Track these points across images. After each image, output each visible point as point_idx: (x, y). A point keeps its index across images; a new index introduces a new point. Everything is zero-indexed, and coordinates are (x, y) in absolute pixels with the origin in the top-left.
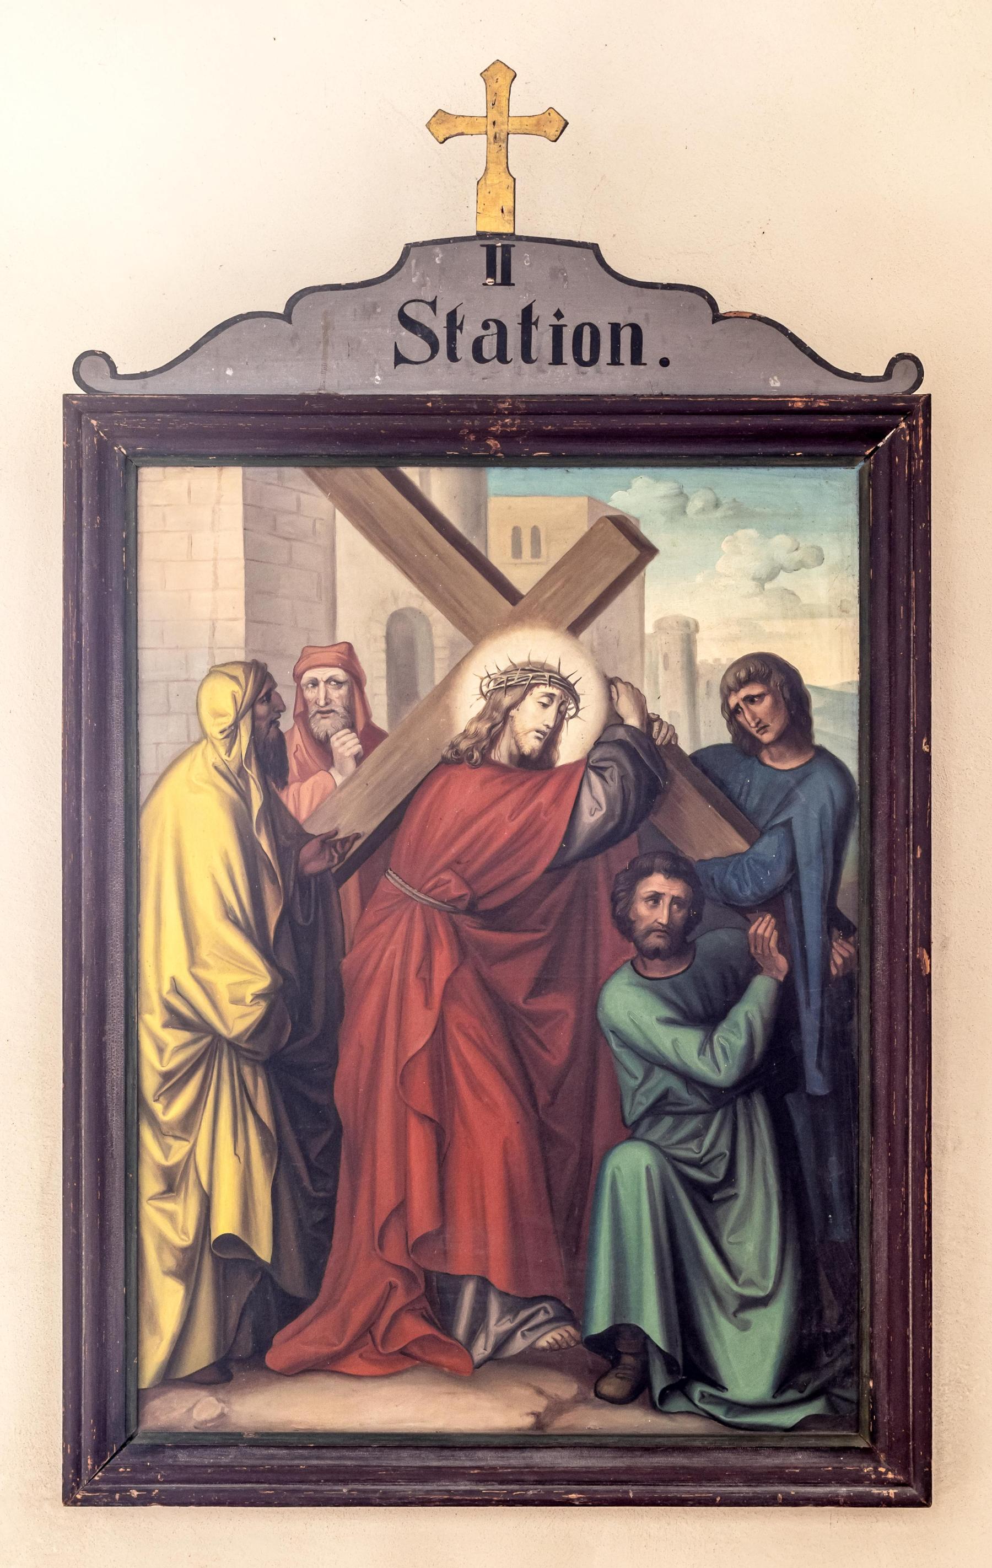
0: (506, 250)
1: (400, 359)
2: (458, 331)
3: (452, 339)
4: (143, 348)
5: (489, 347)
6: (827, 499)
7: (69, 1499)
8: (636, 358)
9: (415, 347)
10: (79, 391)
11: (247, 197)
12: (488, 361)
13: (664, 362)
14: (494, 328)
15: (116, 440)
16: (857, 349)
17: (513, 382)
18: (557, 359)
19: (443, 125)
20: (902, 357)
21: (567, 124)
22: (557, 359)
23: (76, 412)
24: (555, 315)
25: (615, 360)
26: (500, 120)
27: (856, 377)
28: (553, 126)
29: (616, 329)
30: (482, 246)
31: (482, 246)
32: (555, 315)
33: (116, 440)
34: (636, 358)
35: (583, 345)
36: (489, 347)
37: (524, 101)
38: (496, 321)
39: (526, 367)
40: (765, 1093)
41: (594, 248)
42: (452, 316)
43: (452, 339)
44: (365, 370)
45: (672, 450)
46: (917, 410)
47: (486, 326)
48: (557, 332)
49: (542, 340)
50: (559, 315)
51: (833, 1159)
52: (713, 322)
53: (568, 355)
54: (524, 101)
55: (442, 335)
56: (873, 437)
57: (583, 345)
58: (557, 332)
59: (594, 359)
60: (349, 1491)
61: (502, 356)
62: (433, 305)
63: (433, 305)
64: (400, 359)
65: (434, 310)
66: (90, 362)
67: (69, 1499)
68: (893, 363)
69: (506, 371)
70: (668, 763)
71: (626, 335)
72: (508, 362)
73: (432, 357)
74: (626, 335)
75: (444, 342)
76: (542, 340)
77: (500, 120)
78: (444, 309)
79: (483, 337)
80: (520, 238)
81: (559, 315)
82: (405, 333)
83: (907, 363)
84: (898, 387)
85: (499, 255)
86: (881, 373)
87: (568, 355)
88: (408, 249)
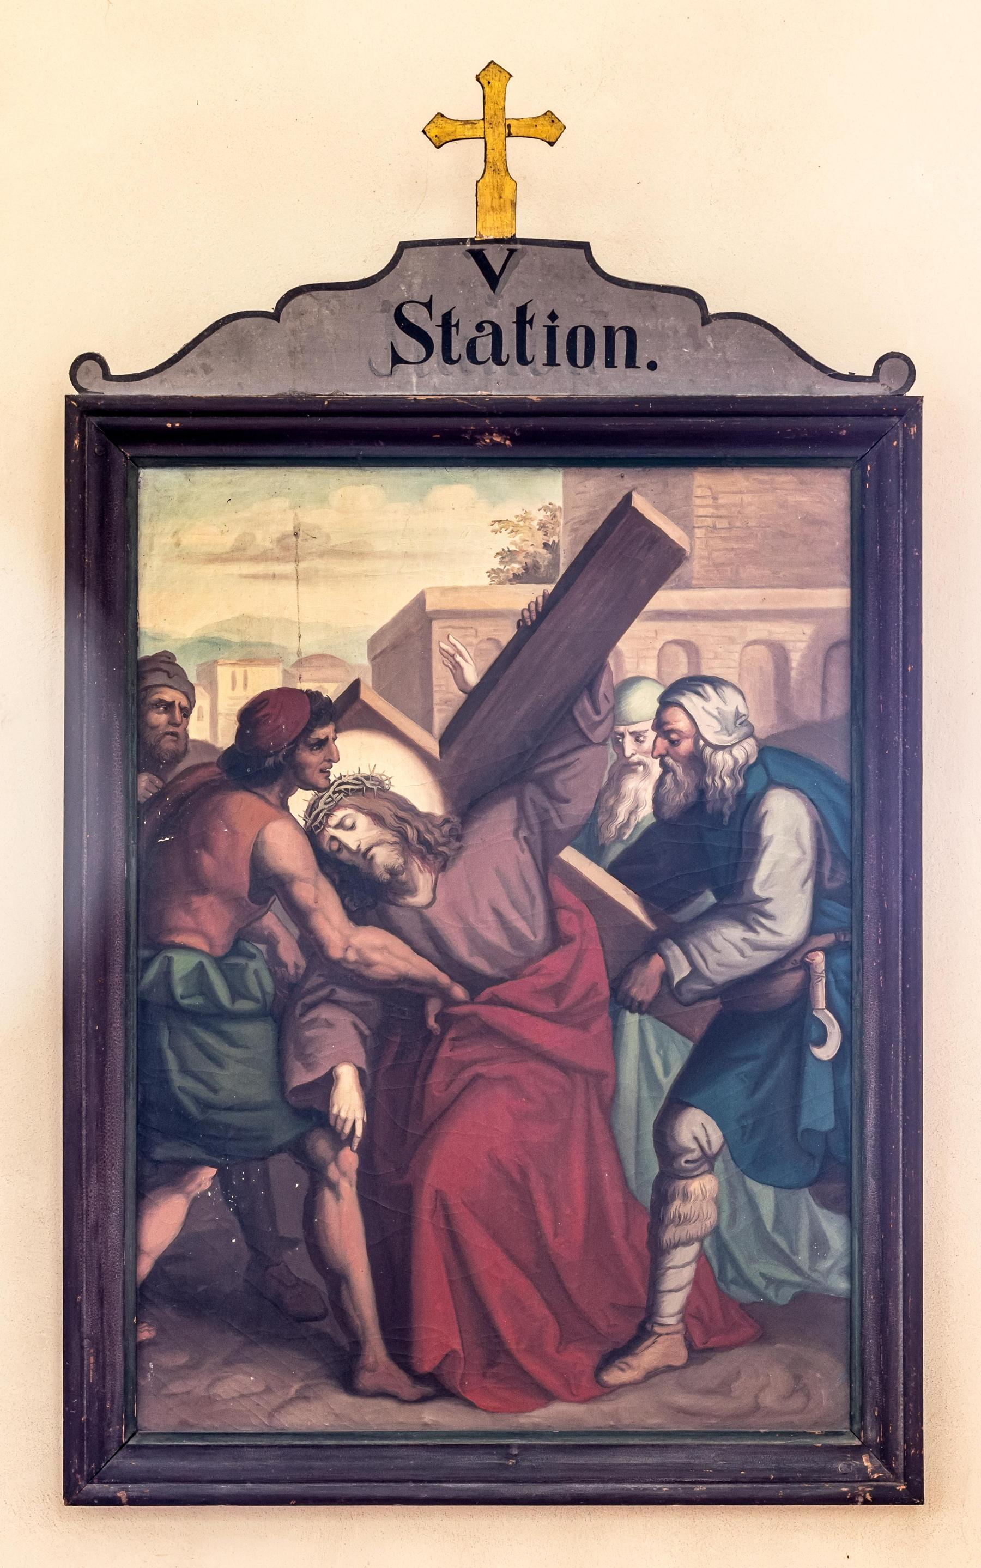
1: (397, 359)
4: (139, 348)
5: (484, 347)
6: (819, 497)
7: (73, 1496)
8: (631, 362)
9: (410, 348)
10: (76, 393)
12: (621, 328)
13: (652, 366)
14: (488, 329)
15: (119, 440)
16: (846, 348)
18: (551, 361)
19: (441, 132)
22: (551, 361)
25: (610, 364)
26: (493, 125)
27: (852, 378)
28: (549, 128)
29: (610, 332)
33: (119, 440)
34: (631, 362)
35: (579, 347)
37: (466, 104)
39: (496, 368)
42: (447, 317)
45: (817, 452)
46: (910, 411)
47: (480, 327)
48: (551, 332)
50: (553, 316)
54: (520, 104)
55: (436, 337)
56: (862, 436)
58: (551, 332)
59: (589, 360)
62: (428, 306)
63: (428, 306)
64: (397, 359)
67: (73, 1496)
68: (881, 361)
71: (621, 341)
74: (621, 341)
77: (493, 125)
78: (438, 312)
79: (475, 338)
80: (524, 241)
83: (897, 365)
85: (489, 259)
88: (403, 246)
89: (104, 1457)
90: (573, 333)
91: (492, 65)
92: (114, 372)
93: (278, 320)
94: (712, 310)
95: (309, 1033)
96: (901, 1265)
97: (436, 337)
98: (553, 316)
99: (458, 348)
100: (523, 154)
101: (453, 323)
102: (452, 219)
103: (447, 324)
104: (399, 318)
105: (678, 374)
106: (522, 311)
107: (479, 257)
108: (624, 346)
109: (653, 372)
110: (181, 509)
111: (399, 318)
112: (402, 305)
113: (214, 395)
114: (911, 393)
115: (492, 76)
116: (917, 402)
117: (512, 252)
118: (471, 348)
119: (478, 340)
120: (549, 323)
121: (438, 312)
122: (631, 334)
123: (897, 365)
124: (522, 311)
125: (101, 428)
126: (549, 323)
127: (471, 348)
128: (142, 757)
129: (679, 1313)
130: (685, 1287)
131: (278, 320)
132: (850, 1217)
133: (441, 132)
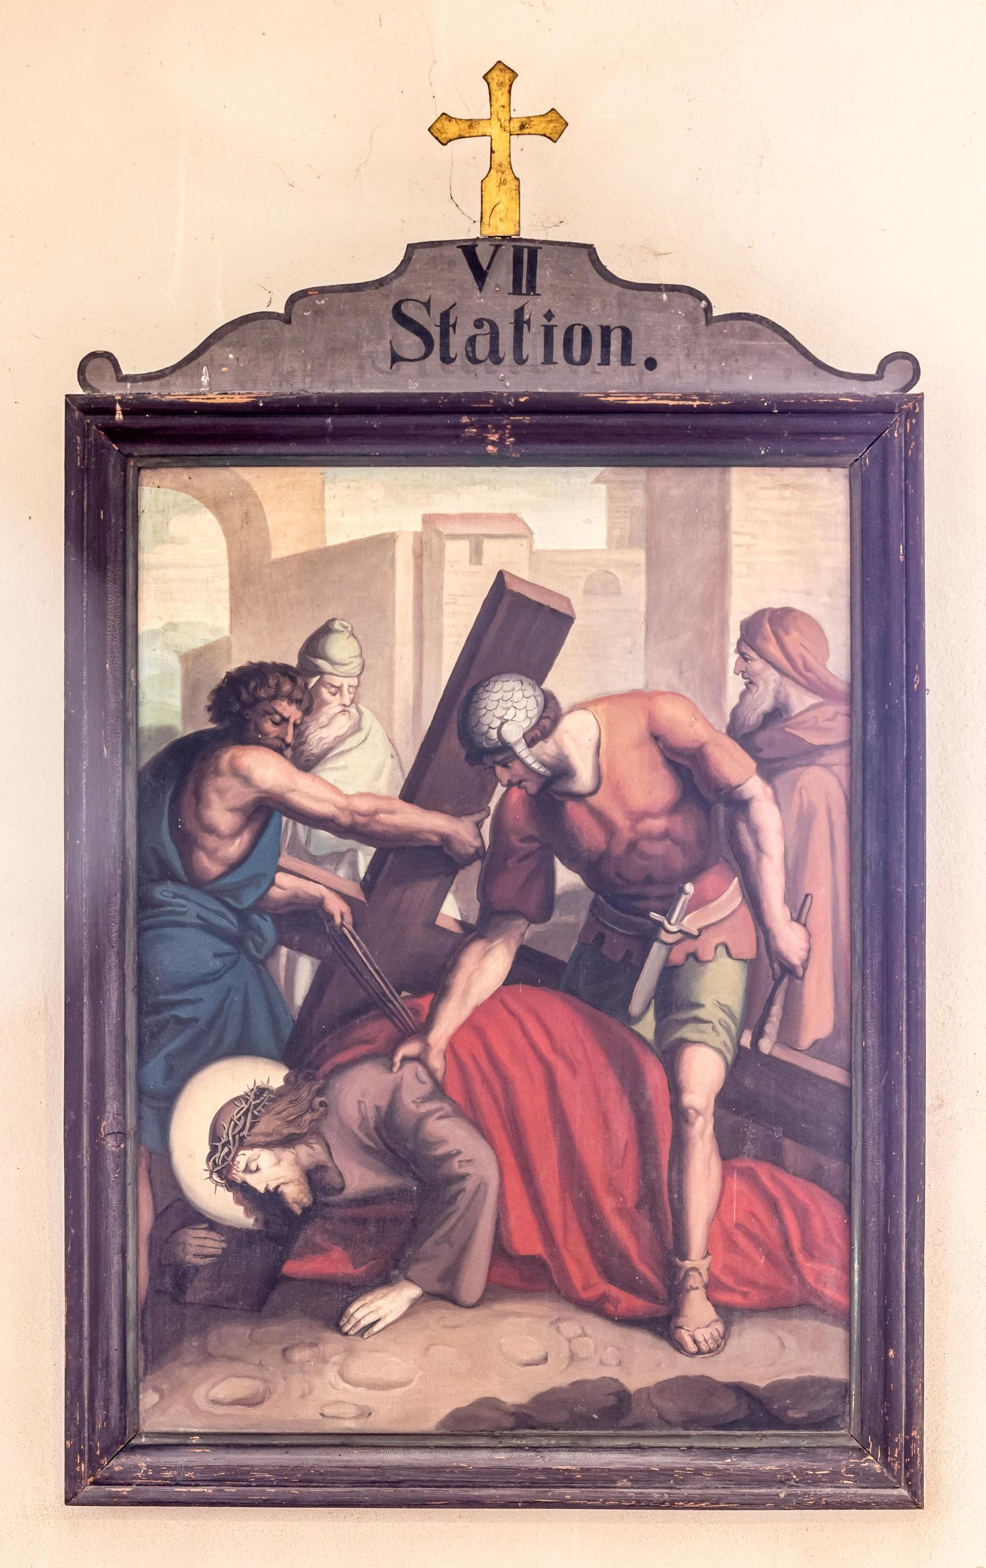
0: (533, 253)
1: (396, 359)
3: (445, 335)
4: (150, 348)
7: (71, 1499)
8: (626, 358)
9: (410, 344)
10: (80, 391)
14: (487, 328)
15: (123, 439)
16: (850, 347)
18: (548, 359)
21: (515, 75)
24: (545, 316)
25: (605, 361)
28: (554, 125)
29: (606, 332)
32: (545, 316)
33: (123, 439)
34: (626, 358)
35: (581, 344)
37: (472, 102)
38: (488, 321)
40: (296, 1216)
41: (590, 250)
42: (445, 316)
43: (445, 335)
47: (479, 324)
49: (533, 345)
52: (549, 311)
55: (435, 333)
56: (866, 436)
57: (581, 344)
60: (788, 1495)
61: (495, 357)
62: (427, 305)
63: (427, 305)
69: (502, 371)
72: (454, 360)
73: (425, 356)
75: (435, 339)
76: (533, 345)
77: (505, 114)
78: (437, 311)
79: (475, 336)
82: (401, 330)
83: (905, 363)
84: (885, 389)
85: (525, 259)
87: (615, 358)
89: (106, 1455)
90: (570, 330)
91: (508, 75)
96: (905, 1171)
97: (435, 333)
98: (549, 315)
99: (457, 343)
100: (528, 153)
105: (683, 376)
106: (519, 312)
108: (620, 343)
109: (658, 359)
113: (395, 391)
114: (914, 391)
116: (919, 399)
117: (498, 247)
119: (478, 338)
120: (545, 322)
122: (627, 335)
123: (905, 363)
126: (545, 322)
129: (688, 1291)
132: (849, 1327)
133: (444, 130)
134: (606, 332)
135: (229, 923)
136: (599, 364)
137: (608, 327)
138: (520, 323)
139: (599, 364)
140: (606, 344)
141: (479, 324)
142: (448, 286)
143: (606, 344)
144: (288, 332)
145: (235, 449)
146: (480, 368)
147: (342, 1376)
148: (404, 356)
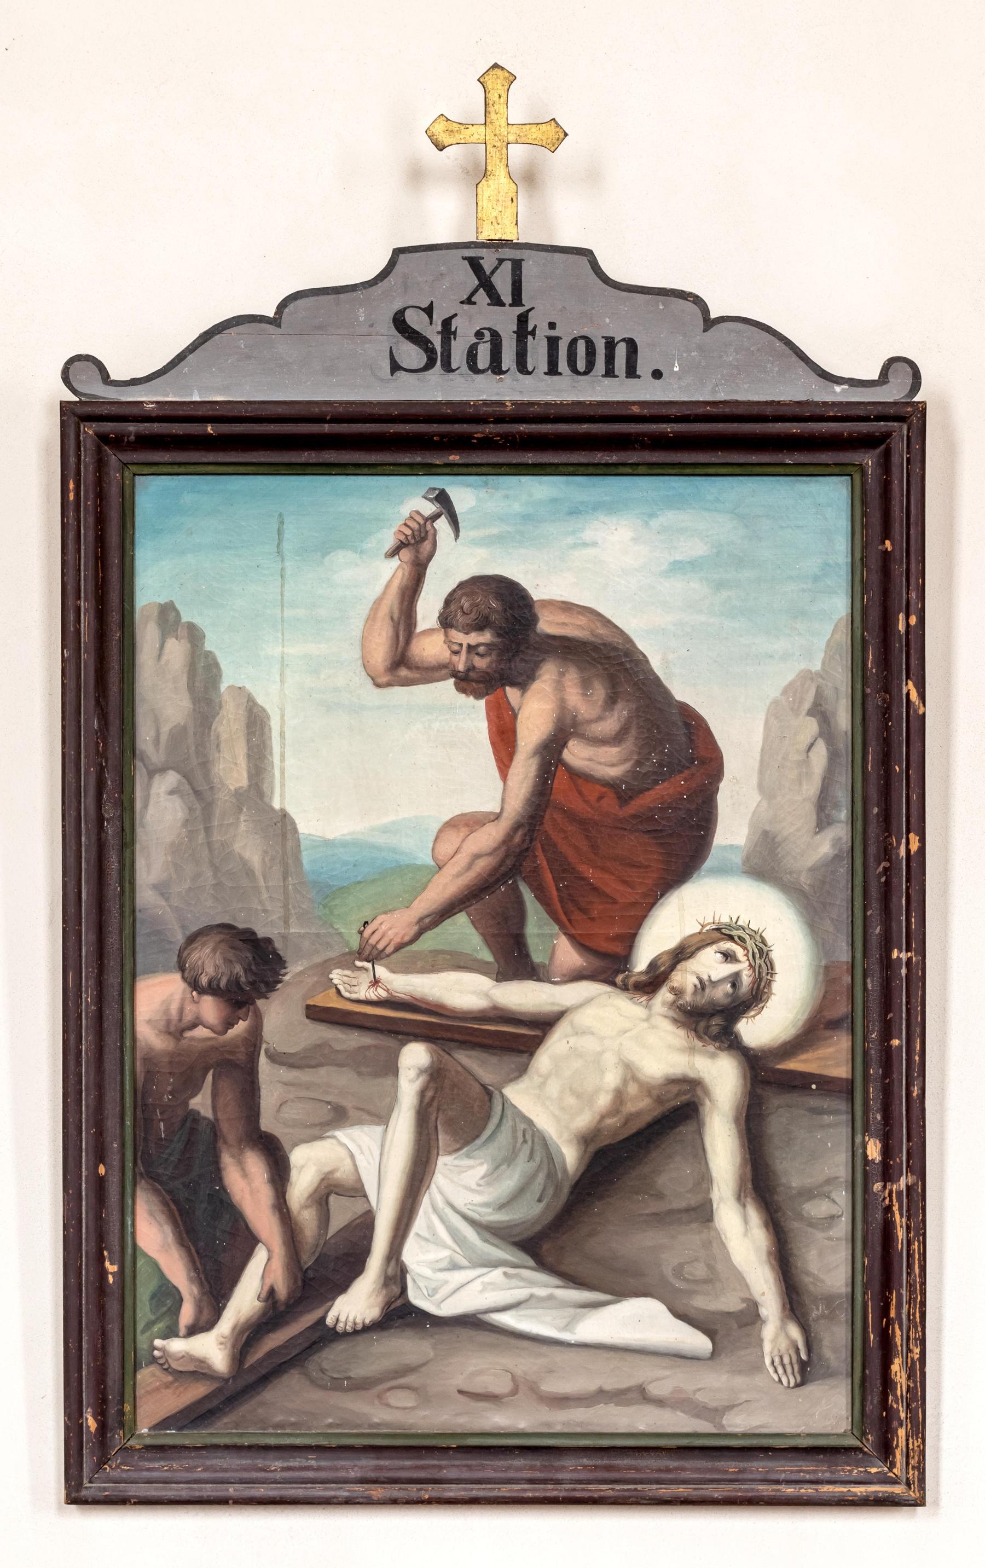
0: (517, 265)
1: (395, 367)
2: (530, 337)
3: (446, 343)
4: (138, 348)
6: (814, 515)
7: (76, 1496)
9: (412, 355)
11: (242, 221)
13: (657, 374)
14: (487, 333)
15: (118, 445)
16: (848, 348)
17: (489, 382)
18: (553, 370)
20: (892, 361)
21: (496, 66)
22: (553, 370)
23: (75, 417)
26: (496, 130)
29: (610, 344)
30: (464, 258)
31: (464, 258)
33: (118, 445)
34: (631, 372)
36: (483, 360)
37: (518, 109)
38: (489, 329)
42: (447, 323)
43: (446, 343)
44: (362, 376)
51: (71, 482)
52: (705, 331)
53: (563, 365)
55: (437, 342)
56: (868, 445)
58: (553, 343)
61: (496, 367)
63: (429, 311)
65: (431, 317)
66: (77, 367)
67: (76, 1496)
70: (582, 868)
71: (621, 351)
74: (621, 351)
77: (496, 130)
78: (438, 318)
81: (552, 326)
83: (902, 368)
84: (891, 394)
85: (494, 269)
86: (875, 377)
89: (107, 1452)
90: (574, 342)
92: (113, 377)
93: (279, 326)
94: (713, 315)
95: (663, 1256)
97: (437, 342)
101: (530, 329)
102: (443, 219)
103: (447, 331)
104: (399, 322)
105: (679, 379)
106: (523, 320)
107: (474, 263)
109: (651, 371)
110: (155, 496)
111: (399, 322)
112: (405, 309)
114: (917, 399)
115: (497, 76)
116: (921, 410)
118: (472, 355)
121: (438, 318)
122: (632, 345)
124: (523, 320)
125: (103, 438)
127: (472, 355)
128: (460, 1068)
130: (75, 392)
131: (279, 326)
132: (135, 1245)
134: (610, 344)
135: (371, 957)
136: (545, 373)
137: (613, 338)
138: (523, 331)
139: (545, 373)
140: (610, 358)
141: (479, 334)
142: (450, 288)
143: (610, 358)
144: (699, 337)
145: (454, 458)
146: (479, 378)
147: (517, 1386)
148: (404, 365)
